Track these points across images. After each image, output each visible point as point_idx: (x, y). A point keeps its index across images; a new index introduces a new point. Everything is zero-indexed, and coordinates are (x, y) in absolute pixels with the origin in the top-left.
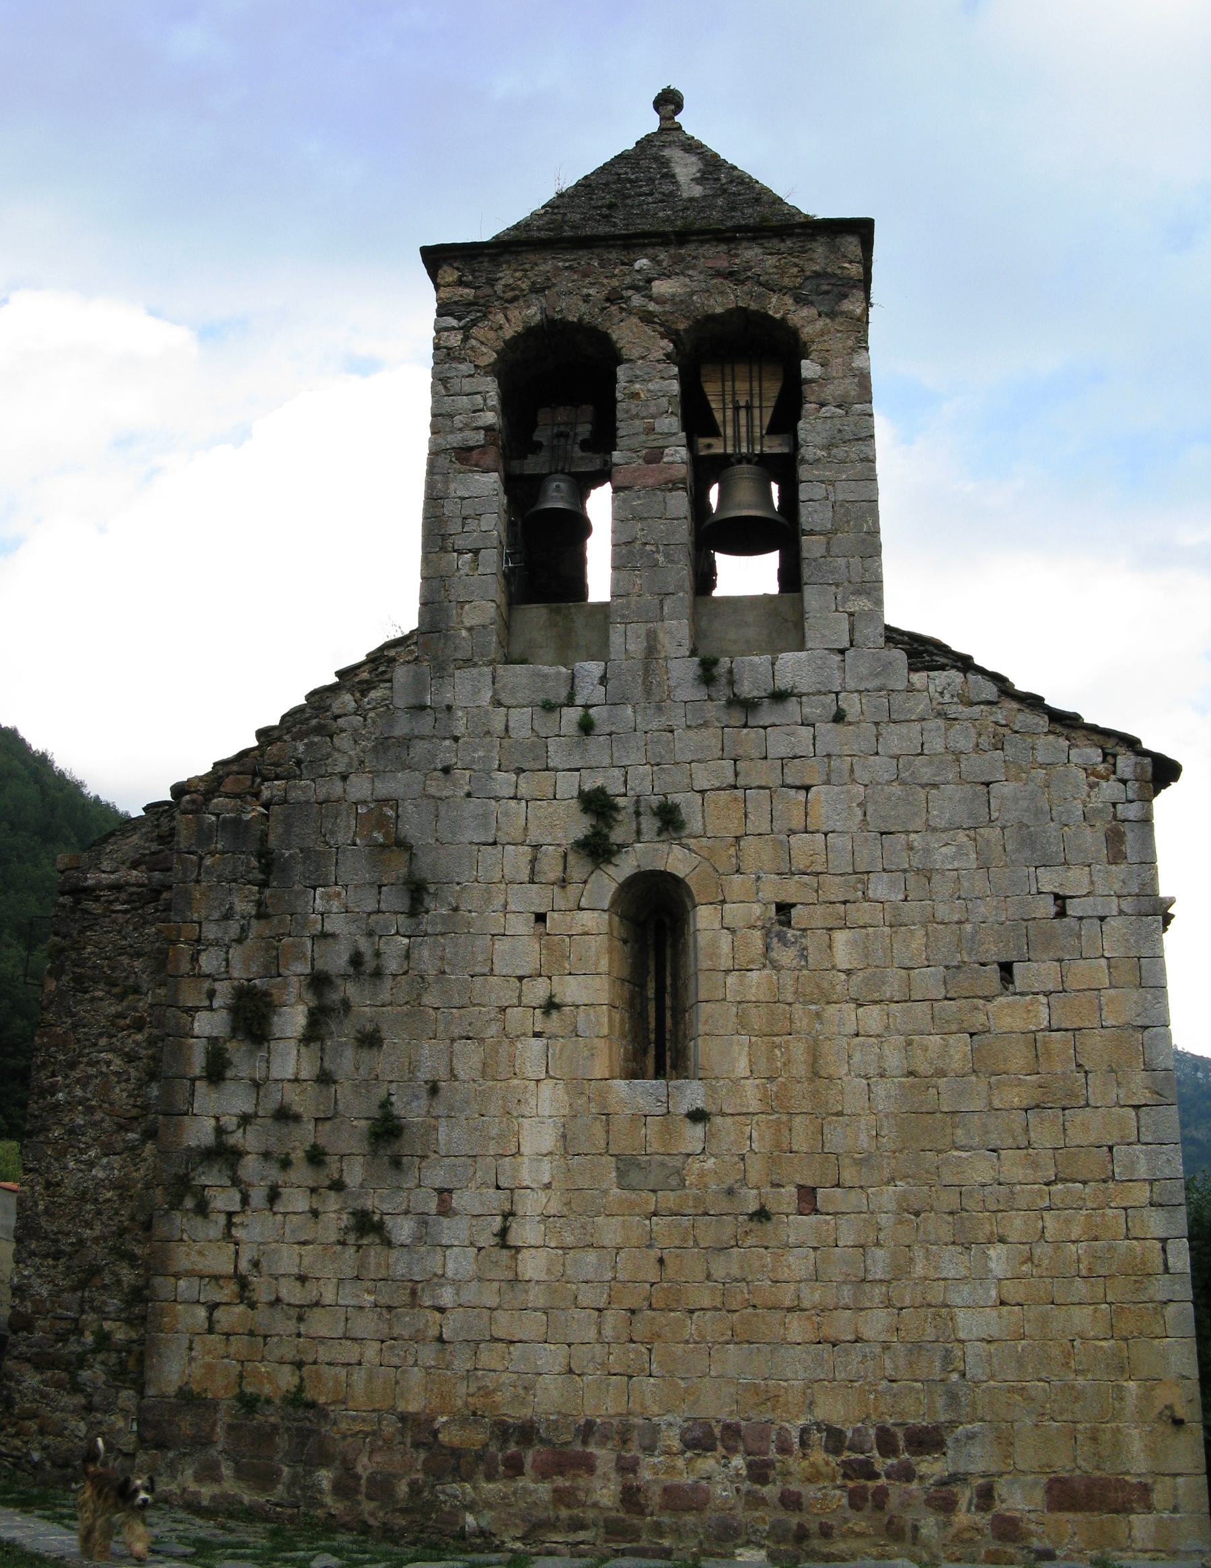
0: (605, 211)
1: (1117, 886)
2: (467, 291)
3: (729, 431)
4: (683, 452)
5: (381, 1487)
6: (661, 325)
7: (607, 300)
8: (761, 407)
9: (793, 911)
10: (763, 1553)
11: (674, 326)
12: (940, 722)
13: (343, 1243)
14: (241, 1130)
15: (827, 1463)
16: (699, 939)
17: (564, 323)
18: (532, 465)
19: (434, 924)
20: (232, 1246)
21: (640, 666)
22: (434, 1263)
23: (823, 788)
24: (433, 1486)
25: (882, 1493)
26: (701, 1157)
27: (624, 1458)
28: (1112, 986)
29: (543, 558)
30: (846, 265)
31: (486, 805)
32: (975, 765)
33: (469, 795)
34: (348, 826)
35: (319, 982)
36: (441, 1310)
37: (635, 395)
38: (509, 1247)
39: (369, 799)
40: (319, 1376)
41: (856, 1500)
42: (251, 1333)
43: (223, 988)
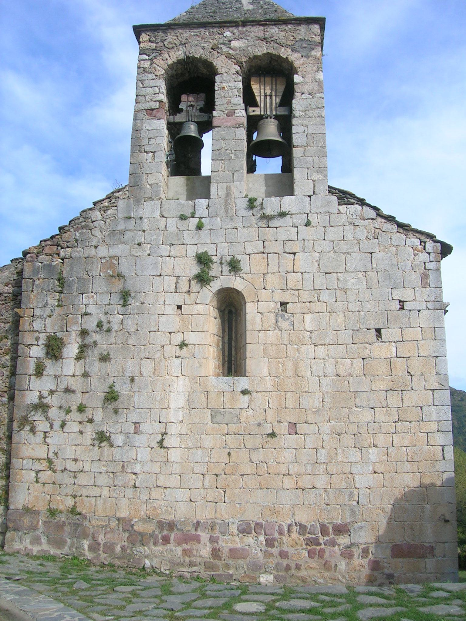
0: (212, 14)
1: (426, 297)
2: (152, 44)
3: (262, 105)
4: (244, 112)
5: (109, 548)
6: (235, 59)
7: (212, 49)
8: (276, 95)
9: (287, 305)
10: (272, 576)
11: (240, 60)
12: (352, 227)
13: (93, 445)
14: (50, 397)
15: (299, 539)
16: (247, 317)
17: (194, 58)
18: (179, 118)
19: (133, 309)
20: (47, 447)
21: (223, 200)
22: (132, 454)
23: (301, 254)
24: (132, 548)
25: (322, 552)
26: (247, 410)
27: (213, 537)
28: (423, 339)
29: (184, 158)
30: (313, 36)
31: (157, 259)
32: (367, 245)
33: (149, 255)
34: (97, 267)
35: (84, 333)
36: (135, 474)
37: (223, 88)
38: (164, 448)
39: (107, 256)
40: (83, 501)
41: (311, 554)
42: (54, 483)
43: (43, 336)
